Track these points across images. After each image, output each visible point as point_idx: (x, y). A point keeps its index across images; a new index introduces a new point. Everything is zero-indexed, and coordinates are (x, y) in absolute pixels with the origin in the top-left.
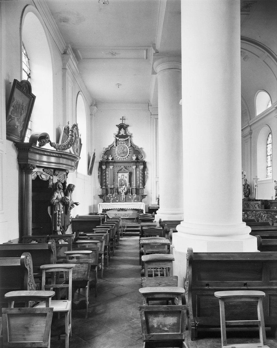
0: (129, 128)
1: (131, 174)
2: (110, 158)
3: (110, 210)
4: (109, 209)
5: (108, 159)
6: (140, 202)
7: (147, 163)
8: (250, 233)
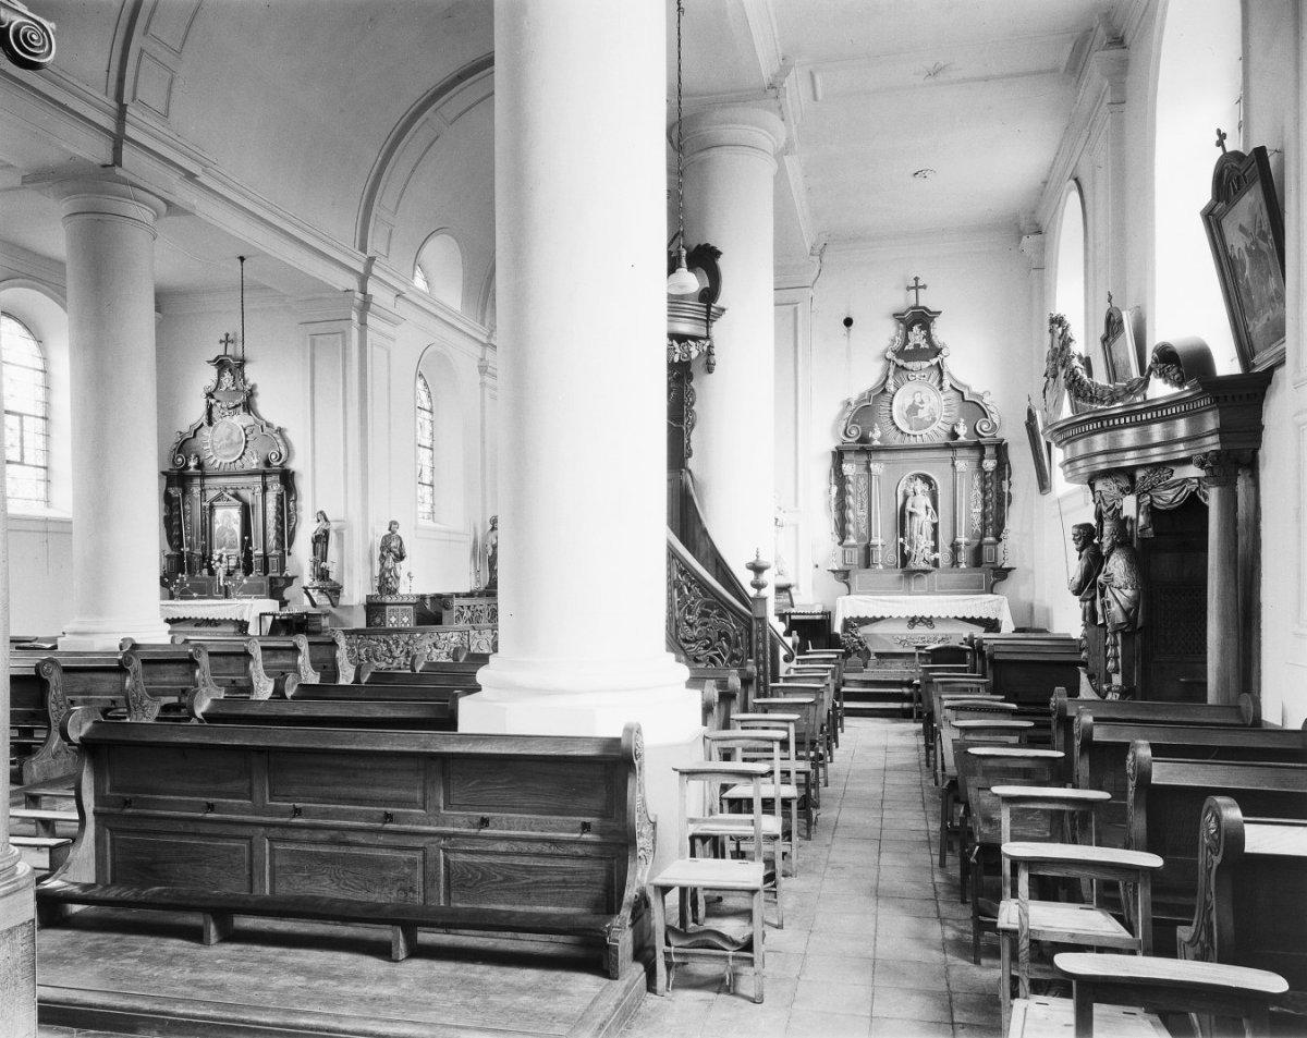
0: (248, 369)
1: (246, 511)
2: (192, 463)
3: (875, 620)
4: (878, 616)
5: (187, 467)
6: (986, 592)
7: (296, 475)
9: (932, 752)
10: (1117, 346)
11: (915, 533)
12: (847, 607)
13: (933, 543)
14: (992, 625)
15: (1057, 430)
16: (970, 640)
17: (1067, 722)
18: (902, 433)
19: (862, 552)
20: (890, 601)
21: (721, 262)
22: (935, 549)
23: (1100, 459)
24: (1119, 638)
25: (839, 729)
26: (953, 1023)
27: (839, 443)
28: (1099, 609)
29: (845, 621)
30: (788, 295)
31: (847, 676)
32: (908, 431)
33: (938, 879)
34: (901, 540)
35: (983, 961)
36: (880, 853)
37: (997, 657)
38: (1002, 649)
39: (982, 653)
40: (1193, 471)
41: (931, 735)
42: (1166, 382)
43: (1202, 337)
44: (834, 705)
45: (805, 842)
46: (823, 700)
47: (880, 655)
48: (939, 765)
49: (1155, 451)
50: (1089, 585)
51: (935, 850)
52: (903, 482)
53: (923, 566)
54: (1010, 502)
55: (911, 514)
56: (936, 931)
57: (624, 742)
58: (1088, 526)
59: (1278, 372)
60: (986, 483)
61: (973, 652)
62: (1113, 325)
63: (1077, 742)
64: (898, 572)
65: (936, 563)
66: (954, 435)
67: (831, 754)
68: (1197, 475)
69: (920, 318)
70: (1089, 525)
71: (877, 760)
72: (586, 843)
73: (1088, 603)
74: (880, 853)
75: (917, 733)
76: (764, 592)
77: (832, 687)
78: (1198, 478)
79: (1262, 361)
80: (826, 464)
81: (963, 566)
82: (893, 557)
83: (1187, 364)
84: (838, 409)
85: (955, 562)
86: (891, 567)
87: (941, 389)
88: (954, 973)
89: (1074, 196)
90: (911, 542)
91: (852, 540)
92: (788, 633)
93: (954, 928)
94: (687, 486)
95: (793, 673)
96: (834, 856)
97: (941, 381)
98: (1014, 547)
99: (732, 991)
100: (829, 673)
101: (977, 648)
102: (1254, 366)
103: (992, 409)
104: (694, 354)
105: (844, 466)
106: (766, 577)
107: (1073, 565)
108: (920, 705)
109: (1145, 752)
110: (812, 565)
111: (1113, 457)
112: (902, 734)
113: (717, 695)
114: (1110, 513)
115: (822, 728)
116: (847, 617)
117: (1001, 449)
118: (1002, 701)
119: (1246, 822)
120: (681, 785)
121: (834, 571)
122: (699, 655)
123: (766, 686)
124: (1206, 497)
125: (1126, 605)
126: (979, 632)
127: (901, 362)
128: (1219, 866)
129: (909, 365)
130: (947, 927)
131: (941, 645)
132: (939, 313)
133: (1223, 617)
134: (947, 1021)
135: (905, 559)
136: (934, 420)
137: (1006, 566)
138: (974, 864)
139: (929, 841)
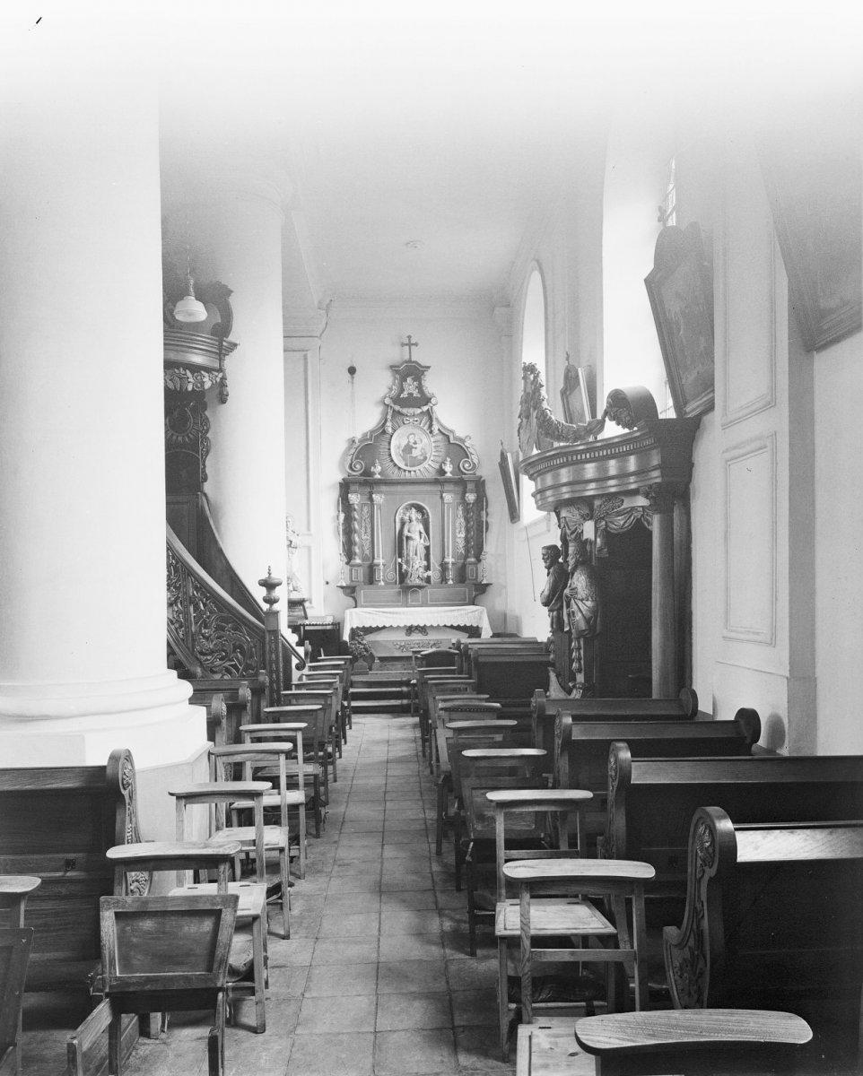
3: (378, 629)
8: (190, 699)
9: (427, 744)
10: (572, 399)
11: (411, 554)
12: (355, 618)
13: (425, 563)
14: (474, 631)
15: (529, 464)
16: (458, 645)
17: (548, 722)
18: (399, 468)
19: (367, 571)
20: (390, 613)
21: (232, 300)
22: (427, 568)
23: (564, 489)
24: (582, 643)
25: (347, 727)
26: (453, 1028)
27: (346, 476)
28: (565, 618)
29: (352, 629)
30: (296, 343)
31: (355, 678)
32: (405, 468)
33: (436, 868)
34: (399, 560)
35: (479, 952)
36: (383, 845)
37: (481, 660)
38: (484, 652)
39: (468, 657)
40: (641, 501)
41: (427, 730)
42: (618, 424)
43: (648, 388)
44: (342, 706)
45: (313, 841)
46: (331, 705)
47: (382, 659)
48: (434, 758)
49: (612, 482)
50: (556, 598)
51: (432, 838)
52: (400, 510)
53: (418, 582)
54: (487, 529)
55: (408, 538)
56: (435, 925)
57: (109, 771)
58: (554, 547)
59: (706, 418)
60: (468, 513)
61: (460, 655)
62: (571, 381)
63: (558, 741)
64: (397, 588)
65: (428, 580)
66: (442, 472)
67: (340, 751)
68: (643, 505)
69: (411, 371)
70: (555, 547)
71: (380, 754)
72: (71, 881)
73: (555, 613)
74: (383, 845)
75: (415, 726)
76: (276, 607)
77: (340, 692)
78: (642, 507)
79: (692, 408)
80: (334, 495)
81: (451, 582)
82: (393, 575)
83: (630, 408)
84: (343, 446)
85: (444, 579)
86: (391, 583)
87: (431, 432)
88: (453, 968)
89: (536, 276)
90: (407, 562)
91: (358, 561)
92: (300, 643)
93: (452, 919)
94: (203, 507)
95: (305, 680)
96: (342, 853)
97: (431, 426)
98: (490, 567)
99: (232, 1023)
100: (337, 679)
101: (464, 652)
102: (686, 413)
103: (471, 450)
104: (208, 385)
105: (350, 495)
106: (279, 592)
107: (542, 581)
108: (417, 701)
109: (568, 720)
110: (323, 582)
111: (577, 487)
112: (402, 727)
113: (224, 708)
114: (573, 536)
115: (331, 728)
116: (354, 627)
117: (480, 485)
118: (487, 700)
119: (736, 829)
120: (178, 810)
121: (342, 587)
122: (215, 667)
123: (278, 694)
124: (649, 524)
125: (588, 614)
126: (464, 639)
127: (397, 408)
128: (711, 879)
129: (405, 411)
130: (444, 919)
131: (434, 649)
132: (429, 367)
133: (664, 625)
134: (447, 1026)
135: (403, 576)
136: (425, 458)
137: (485, 582)
138: (469, 862)
139: (426, 829)
